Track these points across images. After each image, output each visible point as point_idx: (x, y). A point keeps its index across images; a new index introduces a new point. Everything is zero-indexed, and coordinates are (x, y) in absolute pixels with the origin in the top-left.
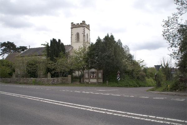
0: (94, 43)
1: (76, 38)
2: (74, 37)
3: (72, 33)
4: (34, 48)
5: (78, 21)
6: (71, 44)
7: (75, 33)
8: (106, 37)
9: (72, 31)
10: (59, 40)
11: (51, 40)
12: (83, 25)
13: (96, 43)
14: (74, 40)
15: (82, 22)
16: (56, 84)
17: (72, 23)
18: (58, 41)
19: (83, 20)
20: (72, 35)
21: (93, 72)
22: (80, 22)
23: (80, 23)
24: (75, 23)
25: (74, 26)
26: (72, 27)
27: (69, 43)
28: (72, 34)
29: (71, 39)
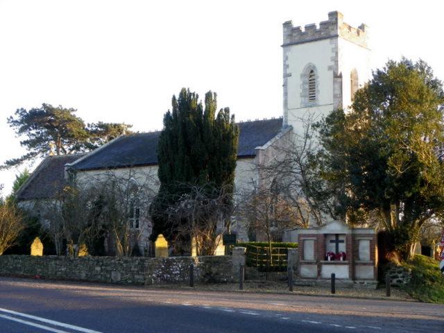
0: (237, 121)
1: (304, 90)
2: (297, 83)
3: (286, 66)
4: (253, 120)
5: (310, 16)
6: (286, 113)
7: (298, 70)
8: (333, 115)
9: (286, 58)
10: (44, 105)
11: (174, 98)
12: (327, 30)
13: (34, 257)
14: (296, 98)
15: (326, 18)
16: (176, 282)
17: (287, 25)
18: (201, 100)
19: (333, 10)
20: (286, 76)
21: (337, 235)
22: (318, 17)
23: (322, 24)
24: (300, 22)
25: (295, 36)
26: (288, 41)
27: (271, 110)
28: (288, 72)
29: (286, 94)
